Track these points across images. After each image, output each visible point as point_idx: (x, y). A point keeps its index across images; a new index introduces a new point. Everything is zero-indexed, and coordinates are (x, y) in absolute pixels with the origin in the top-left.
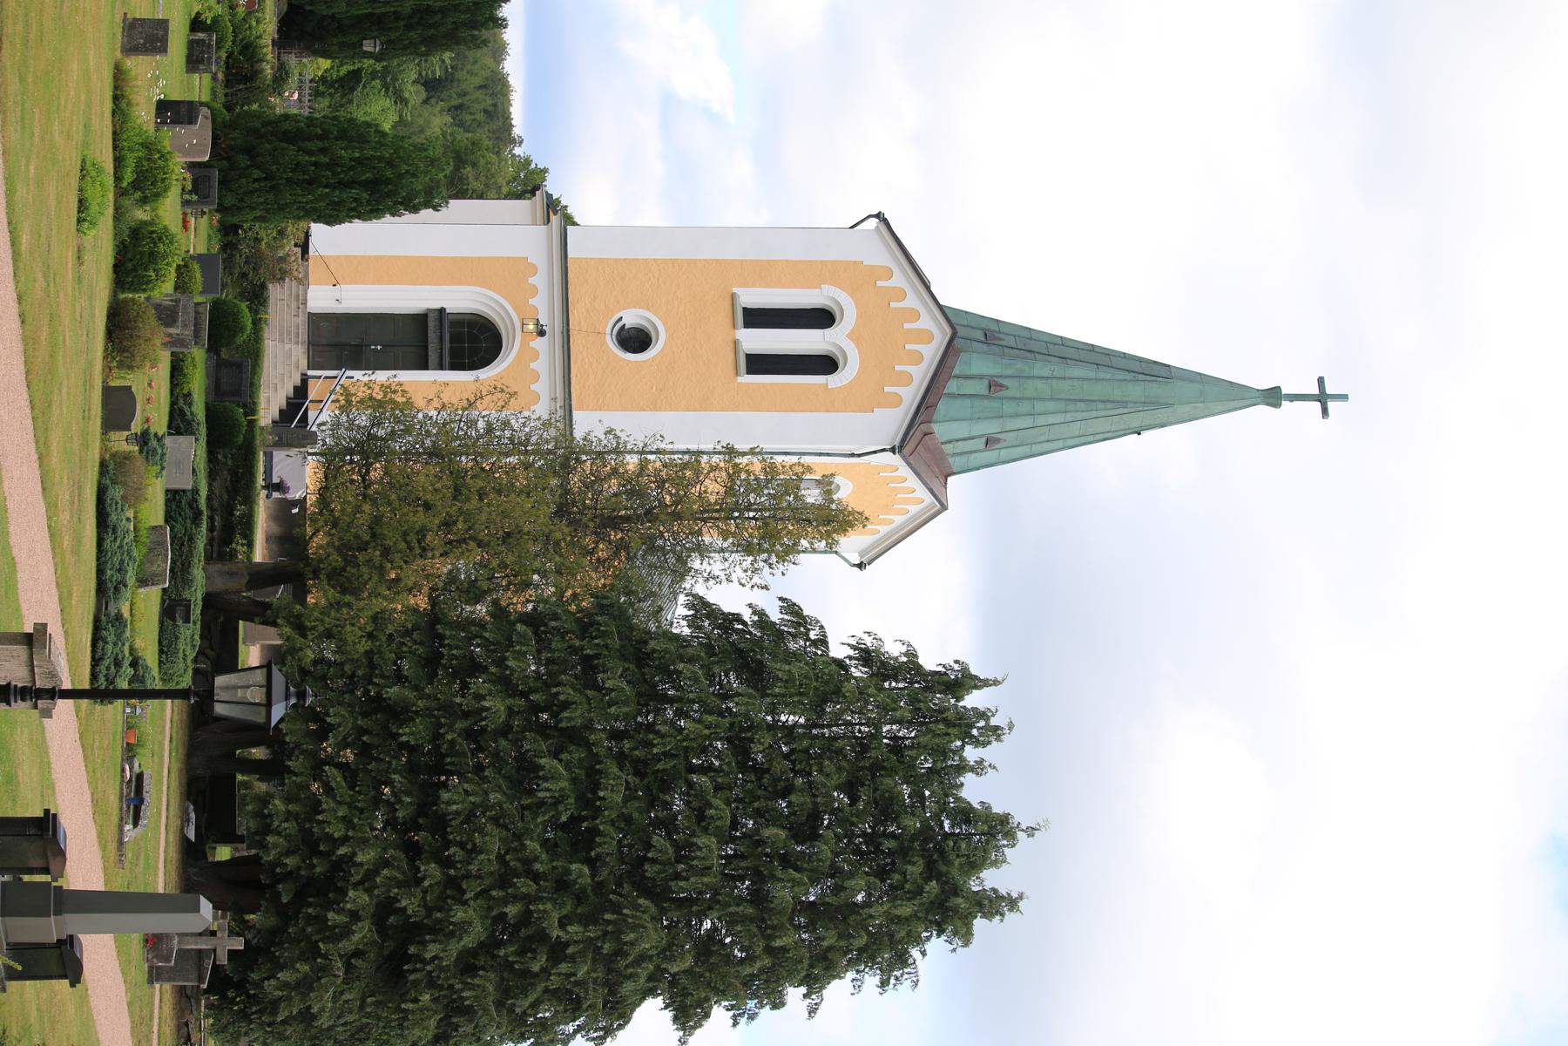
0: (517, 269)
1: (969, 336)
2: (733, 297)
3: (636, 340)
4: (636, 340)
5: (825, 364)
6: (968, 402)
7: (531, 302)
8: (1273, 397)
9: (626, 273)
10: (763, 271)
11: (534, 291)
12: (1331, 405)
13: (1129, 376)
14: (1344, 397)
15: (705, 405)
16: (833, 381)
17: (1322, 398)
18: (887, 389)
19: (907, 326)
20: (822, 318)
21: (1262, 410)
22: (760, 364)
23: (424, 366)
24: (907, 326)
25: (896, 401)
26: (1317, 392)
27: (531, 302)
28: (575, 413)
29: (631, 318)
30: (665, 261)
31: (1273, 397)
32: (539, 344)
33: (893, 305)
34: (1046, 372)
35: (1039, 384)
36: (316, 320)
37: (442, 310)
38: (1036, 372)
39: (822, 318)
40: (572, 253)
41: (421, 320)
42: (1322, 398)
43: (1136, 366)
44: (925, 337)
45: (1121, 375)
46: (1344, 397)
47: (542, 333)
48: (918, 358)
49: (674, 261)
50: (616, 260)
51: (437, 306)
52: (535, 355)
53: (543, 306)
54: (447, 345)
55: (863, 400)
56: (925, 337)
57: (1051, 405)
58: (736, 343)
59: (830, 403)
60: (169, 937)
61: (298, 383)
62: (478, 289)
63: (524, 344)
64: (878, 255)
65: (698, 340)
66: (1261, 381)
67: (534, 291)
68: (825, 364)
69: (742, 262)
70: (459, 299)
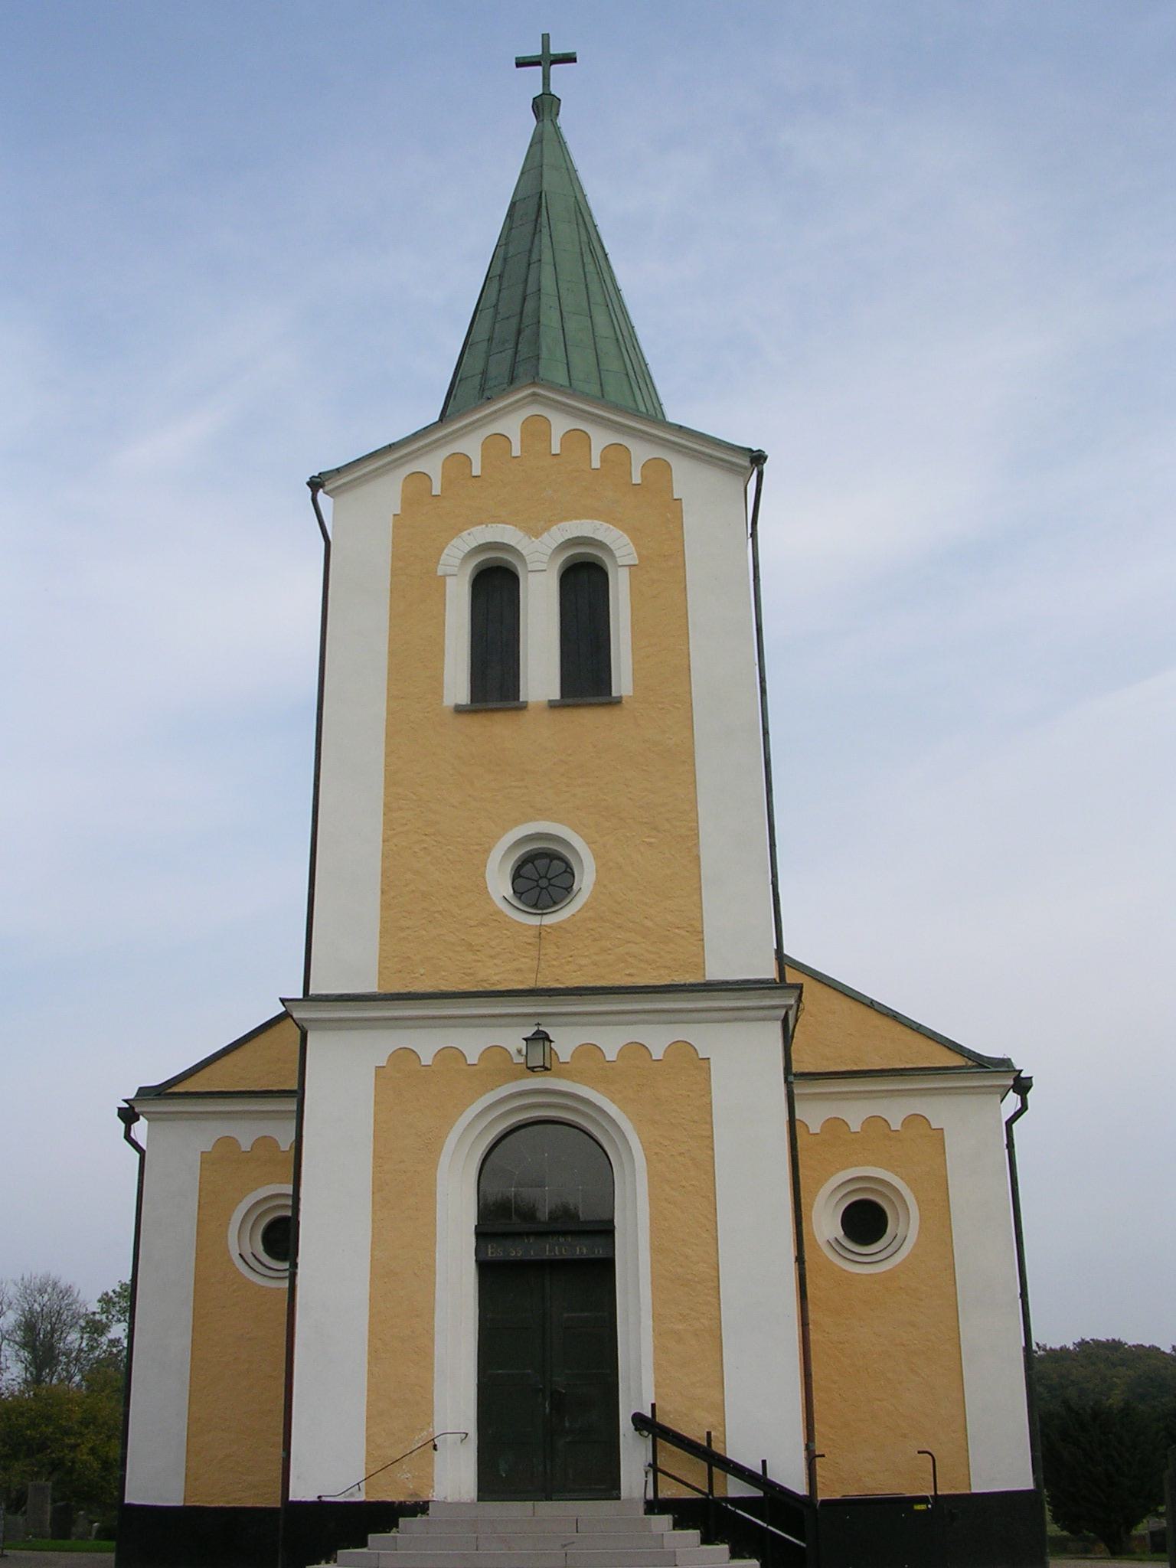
0: (398, 1079)
2: (459, 710)
3: (542, 876)
4: (542, 876)
5: (584, 581)
8: (545, 106)
10: (409, 662)
11: (450, 1055)
12: (555, 49)
14: (546, 38)
15: (680, 759)
16: (622, 550)
17: (547, 60)
18: (637, 479)
19: (516, 451)
20: (495, 585)
21: (566, 119)
26: (539, 69)
28: (715, 972)
29: (499, 885)
30: (388, 823)
31: (545, 106)
32: (565, 1042)
36: (493, 1482)
39: (495, 585)
40: (371, 987)
41: (485, 1268)
44: (536, 431)
45: (536, 242)
46: (546, 38)
48: (577, 439)
49: (388, 809)
50: (385, 907)
52: (590, 1051)
59: (666, 563)
61: (666, 1520)
62: (444, 1160)
63: (565, 1073)
64: (386, 495)
67: (450, 1055)
68: (584, 581)
69: (391, 697)
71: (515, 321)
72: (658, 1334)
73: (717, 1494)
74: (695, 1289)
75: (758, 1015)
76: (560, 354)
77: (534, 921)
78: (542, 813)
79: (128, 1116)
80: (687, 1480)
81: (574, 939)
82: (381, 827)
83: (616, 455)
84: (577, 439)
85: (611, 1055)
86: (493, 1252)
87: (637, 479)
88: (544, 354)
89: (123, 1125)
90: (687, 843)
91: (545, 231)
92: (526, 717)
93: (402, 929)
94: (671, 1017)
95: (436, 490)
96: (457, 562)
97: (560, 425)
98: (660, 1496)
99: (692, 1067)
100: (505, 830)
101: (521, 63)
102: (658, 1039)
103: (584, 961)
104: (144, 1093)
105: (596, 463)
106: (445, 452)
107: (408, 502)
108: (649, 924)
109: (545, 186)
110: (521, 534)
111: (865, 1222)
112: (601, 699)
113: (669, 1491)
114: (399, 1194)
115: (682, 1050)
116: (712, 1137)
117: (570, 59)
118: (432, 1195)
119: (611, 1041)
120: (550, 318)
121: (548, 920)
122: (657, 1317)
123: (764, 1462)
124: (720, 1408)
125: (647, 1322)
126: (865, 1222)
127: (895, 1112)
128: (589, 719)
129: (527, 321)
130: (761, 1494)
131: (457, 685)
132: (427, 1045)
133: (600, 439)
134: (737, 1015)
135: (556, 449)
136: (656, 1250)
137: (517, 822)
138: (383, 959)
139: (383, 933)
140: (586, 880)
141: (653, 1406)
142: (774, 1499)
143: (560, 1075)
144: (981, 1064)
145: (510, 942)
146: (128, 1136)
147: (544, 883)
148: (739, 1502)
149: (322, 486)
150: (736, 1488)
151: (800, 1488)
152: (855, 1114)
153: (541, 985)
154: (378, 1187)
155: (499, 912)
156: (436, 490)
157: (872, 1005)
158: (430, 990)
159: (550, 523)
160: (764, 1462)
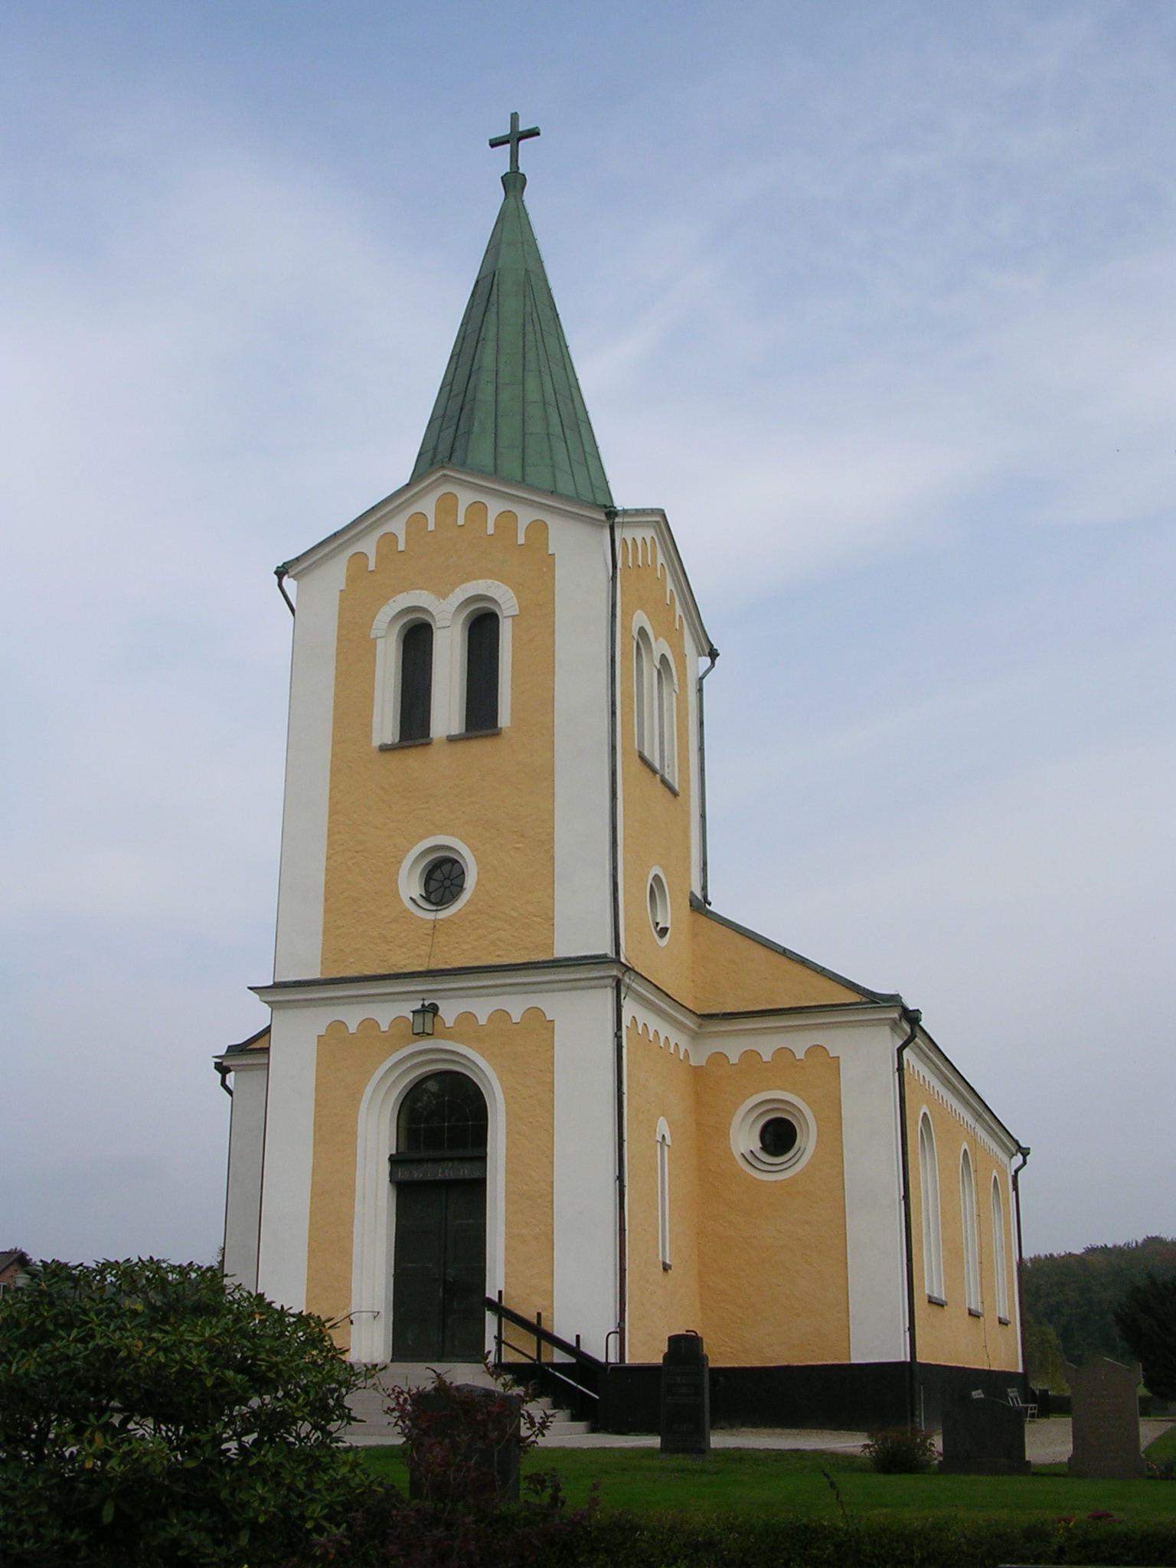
1: (448, 445)
2: (384, 749)
3: (443, 879)
5: (482, 628)
6: (528, 470)
7: (384, 1027)
8: (514, 182)
9: (347, 891)
10: (350, 710)
11: (369, 1024)
12: (523, 127)
13: (492, 317)
14: (514, 117)
15: (545, 775)
16: (507, 603)
17: (515, 138)
18: (521, 540)
20: (417, 638)
21: (530, 197)
22: (481, 713)
23: (478, 1186)
24: (431, 527)
25: (538, 530)
27: (384, 1027)
29: (410, 887)
30: (331, 845)
31: (514, 182)
32: (450, 1011)
33: (401, 547)
34: (491, 388)
35: (504, 396)
37: (393, 1160)
38: (491, 398)
39: (417, 638)
40: (315, 974)
42: (515, 138)
43: (454, 365)
44: (447, 505)
46: (514, 117)
47: (434, 1009)
48: (478, 510)
49: (331, 833)
50: (327, 910)
51: (386, 1167)
52: (468, 1017)
53: (391, 1012)
54: (424, 1154)
55: (537, 567)
56: (447, 505)
57: (532, 384)
58: (452, 739)
60: (955, 1462)
62: (364, 1105)
63: (448, 1034)
64: (335, 574)
65: (448, 798)
66: (497, 196)
67: (369, 1024)
68: (482, 628)
70: (376, 1135)
71: (461, 397)
72: (509, 1236)
73: (543, 1360)
74: (536, 1202)
75: (593, 984)
76: (490, 425)
77: (431, 916)
78: (441, 829)
79: (222, 1069)
80: (522, 1349)
81: (463, 931)
82: (325, 849)
83: (507, 520)
84: (478, 510)
85: (483, 1020)
86: (403, 1175)
87: (521, 540)
88: (476, 428)
89: (219, 1075)
90: (545, 846)
91: (494, 309)
92: (432, 750)
93: (339, 928)
94: (527, 988)
95: (372, 566)
96: (386, 625)
97: (465, 498)
98: (503, 1361)
99: (541, 1026)
100: (413, 845)
101: (494, 144)
102: (516, 1006)
103: (465, 947)
104: (232, 1050)
105: (491, 530)
106: (377, 534)
107: (351, 579)
108: (514, 914)
109: (500, 265)
110: (432, 597)
111: (779, 1136)
112: (489, 731)
113: (509, 1357)
114: (333, 1134)
115: (535, 1014)
116: (552, 1083)
117: (533, 133)
118: (354, 1134)
119: (483, 1009)
120: (486, 393)
121: (443, 915)
122: (509, 1224)
123: (578, 1337)
124: (550, 1294)
125: (501, 1228)
126: (779, 1136)
127: (799, 1044)
128: (479, 748)
129: (468, 398)
130: (574, 1361)
131: (385, 725)
132: (353, 1017)
133: (495, 507)
134: (573, 985)
135: (461, 521)
136: (509, 1171)
137: (422, 838)
138: (325, 951)
139: (326, 931)
140: (470, 882)
141: (500, 1292)
142: (584, 1366)
143: (445, 1037)
144: (873, 1000)
145: (411, 930)
146: (223, 1084)
147: (447, 883)
148: (561, 1367)
149: (287, 572)
150: (560, 1357)
151: (603, 1360)
152: (766, 1047)
153: (433, 967)
154: (318, 1127)
155: (406, 910)
156: (372, 566)
157: (785, 952)
158: (356, 974)
159: (455, 584)
160: (578, 1337)
